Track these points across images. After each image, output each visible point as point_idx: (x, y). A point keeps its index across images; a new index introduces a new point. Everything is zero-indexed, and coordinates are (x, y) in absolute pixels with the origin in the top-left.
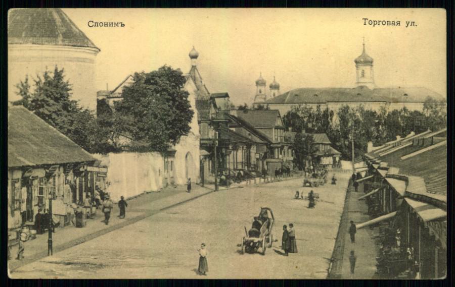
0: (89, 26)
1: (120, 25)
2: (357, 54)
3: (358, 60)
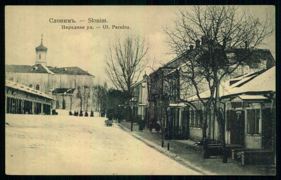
0: (51, 18)
1: (72, 21)
2: (38, 45)
3: (38, 49)
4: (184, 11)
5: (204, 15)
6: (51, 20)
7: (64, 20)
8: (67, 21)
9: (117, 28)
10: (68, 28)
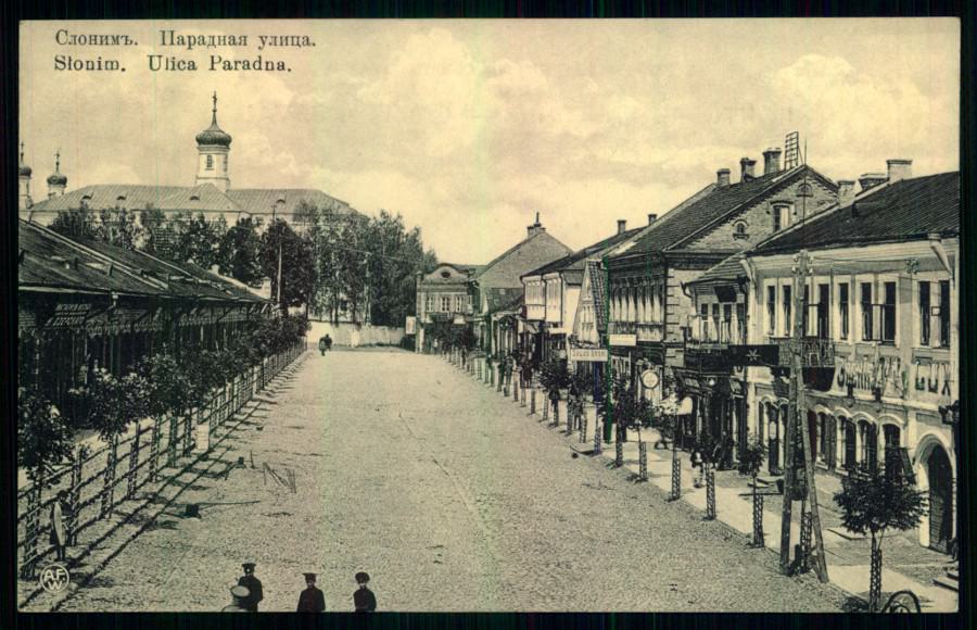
1: (122, 41)
4: (469, 276)
5: (250, 371)
6: (62, 35)
7: (101, 37)
8: (110, 39)
9: (230, 69)
10: (186, 40)
